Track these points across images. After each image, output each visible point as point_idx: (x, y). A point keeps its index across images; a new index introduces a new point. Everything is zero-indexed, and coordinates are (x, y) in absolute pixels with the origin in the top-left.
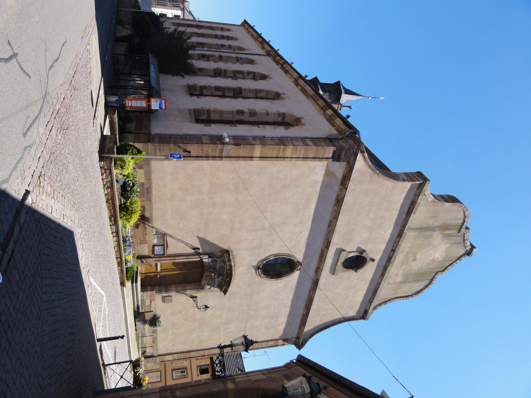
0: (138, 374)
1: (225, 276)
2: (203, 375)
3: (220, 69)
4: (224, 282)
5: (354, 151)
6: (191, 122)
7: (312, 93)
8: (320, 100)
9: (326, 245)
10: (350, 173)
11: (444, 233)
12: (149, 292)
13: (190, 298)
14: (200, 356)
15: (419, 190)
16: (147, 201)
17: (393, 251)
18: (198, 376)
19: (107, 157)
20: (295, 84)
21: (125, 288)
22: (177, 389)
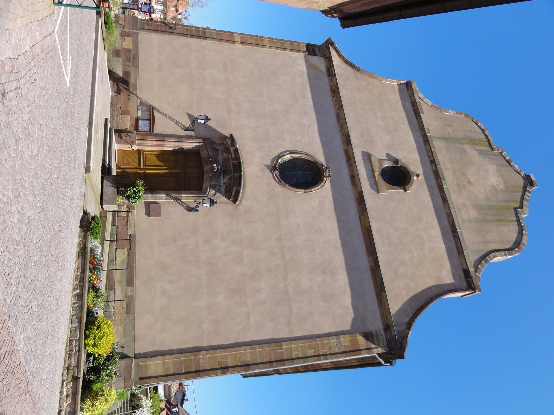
1: (232, 171)
4: (232, 181)
5: (325, 45)
9: (346, 142)
10: (331, 62)
13: (187, 211)
14: (218, 367)
15: (410, 91)
16: (133, 66)
17: (433, 162)
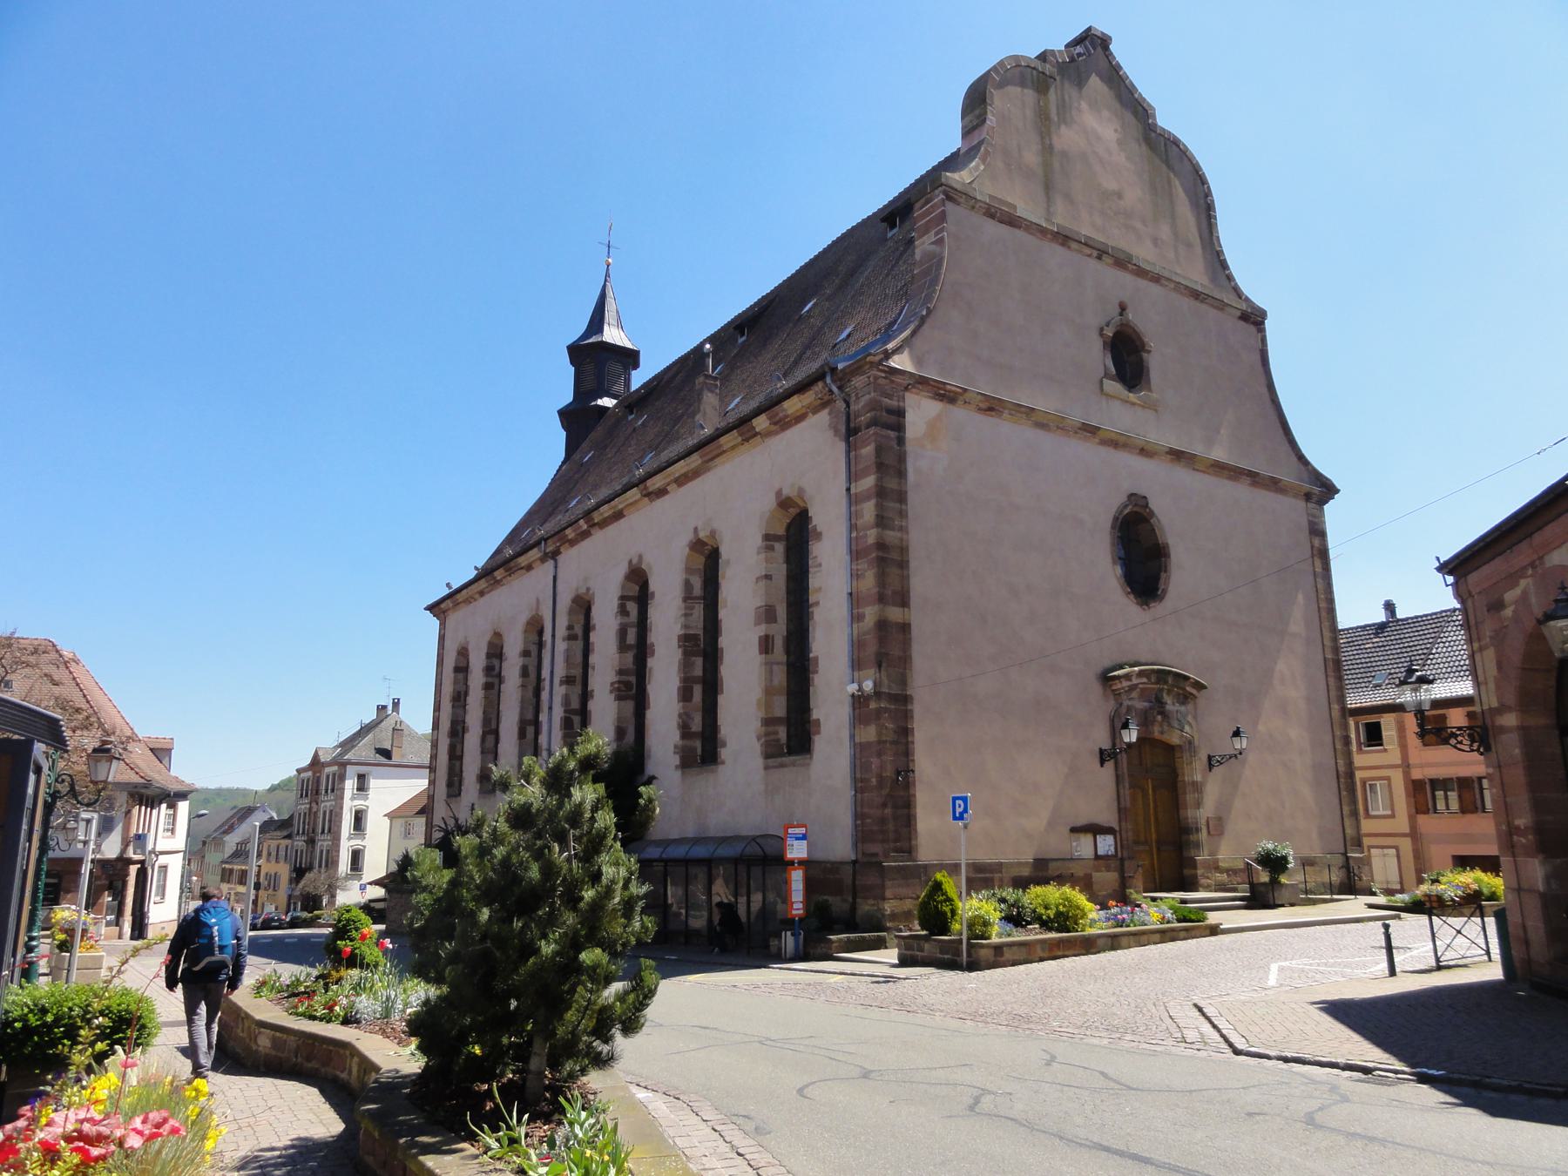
0: (1457, 899)
2: (1384, 737)
3: (616, 686)
5: (883, 375)
6: (809, 765)
7: (697, 460)
8: (722, 443)
11: (1056, 119)
12: (1200, 872)
15: (962, 200)
16: (1001, 872)
18: (1386, 750)
19: (969, 955)
20: (658, 498)
21: (1221, 924)
22: (1508, 823)
